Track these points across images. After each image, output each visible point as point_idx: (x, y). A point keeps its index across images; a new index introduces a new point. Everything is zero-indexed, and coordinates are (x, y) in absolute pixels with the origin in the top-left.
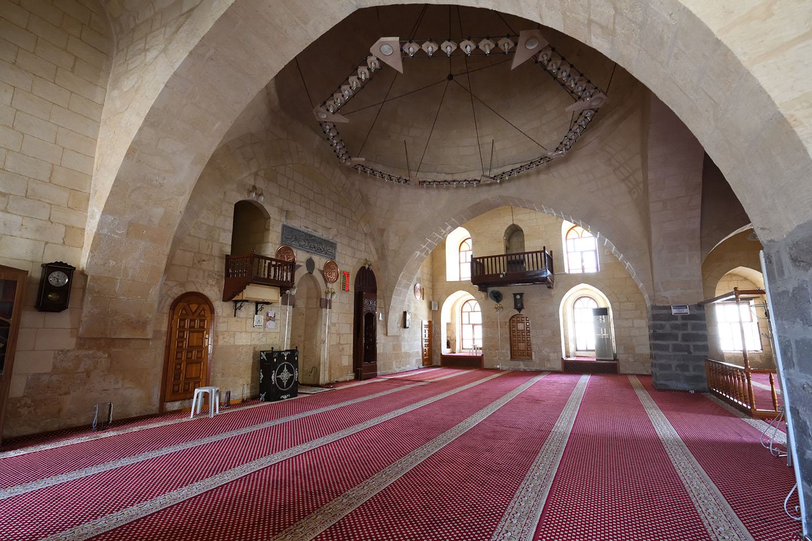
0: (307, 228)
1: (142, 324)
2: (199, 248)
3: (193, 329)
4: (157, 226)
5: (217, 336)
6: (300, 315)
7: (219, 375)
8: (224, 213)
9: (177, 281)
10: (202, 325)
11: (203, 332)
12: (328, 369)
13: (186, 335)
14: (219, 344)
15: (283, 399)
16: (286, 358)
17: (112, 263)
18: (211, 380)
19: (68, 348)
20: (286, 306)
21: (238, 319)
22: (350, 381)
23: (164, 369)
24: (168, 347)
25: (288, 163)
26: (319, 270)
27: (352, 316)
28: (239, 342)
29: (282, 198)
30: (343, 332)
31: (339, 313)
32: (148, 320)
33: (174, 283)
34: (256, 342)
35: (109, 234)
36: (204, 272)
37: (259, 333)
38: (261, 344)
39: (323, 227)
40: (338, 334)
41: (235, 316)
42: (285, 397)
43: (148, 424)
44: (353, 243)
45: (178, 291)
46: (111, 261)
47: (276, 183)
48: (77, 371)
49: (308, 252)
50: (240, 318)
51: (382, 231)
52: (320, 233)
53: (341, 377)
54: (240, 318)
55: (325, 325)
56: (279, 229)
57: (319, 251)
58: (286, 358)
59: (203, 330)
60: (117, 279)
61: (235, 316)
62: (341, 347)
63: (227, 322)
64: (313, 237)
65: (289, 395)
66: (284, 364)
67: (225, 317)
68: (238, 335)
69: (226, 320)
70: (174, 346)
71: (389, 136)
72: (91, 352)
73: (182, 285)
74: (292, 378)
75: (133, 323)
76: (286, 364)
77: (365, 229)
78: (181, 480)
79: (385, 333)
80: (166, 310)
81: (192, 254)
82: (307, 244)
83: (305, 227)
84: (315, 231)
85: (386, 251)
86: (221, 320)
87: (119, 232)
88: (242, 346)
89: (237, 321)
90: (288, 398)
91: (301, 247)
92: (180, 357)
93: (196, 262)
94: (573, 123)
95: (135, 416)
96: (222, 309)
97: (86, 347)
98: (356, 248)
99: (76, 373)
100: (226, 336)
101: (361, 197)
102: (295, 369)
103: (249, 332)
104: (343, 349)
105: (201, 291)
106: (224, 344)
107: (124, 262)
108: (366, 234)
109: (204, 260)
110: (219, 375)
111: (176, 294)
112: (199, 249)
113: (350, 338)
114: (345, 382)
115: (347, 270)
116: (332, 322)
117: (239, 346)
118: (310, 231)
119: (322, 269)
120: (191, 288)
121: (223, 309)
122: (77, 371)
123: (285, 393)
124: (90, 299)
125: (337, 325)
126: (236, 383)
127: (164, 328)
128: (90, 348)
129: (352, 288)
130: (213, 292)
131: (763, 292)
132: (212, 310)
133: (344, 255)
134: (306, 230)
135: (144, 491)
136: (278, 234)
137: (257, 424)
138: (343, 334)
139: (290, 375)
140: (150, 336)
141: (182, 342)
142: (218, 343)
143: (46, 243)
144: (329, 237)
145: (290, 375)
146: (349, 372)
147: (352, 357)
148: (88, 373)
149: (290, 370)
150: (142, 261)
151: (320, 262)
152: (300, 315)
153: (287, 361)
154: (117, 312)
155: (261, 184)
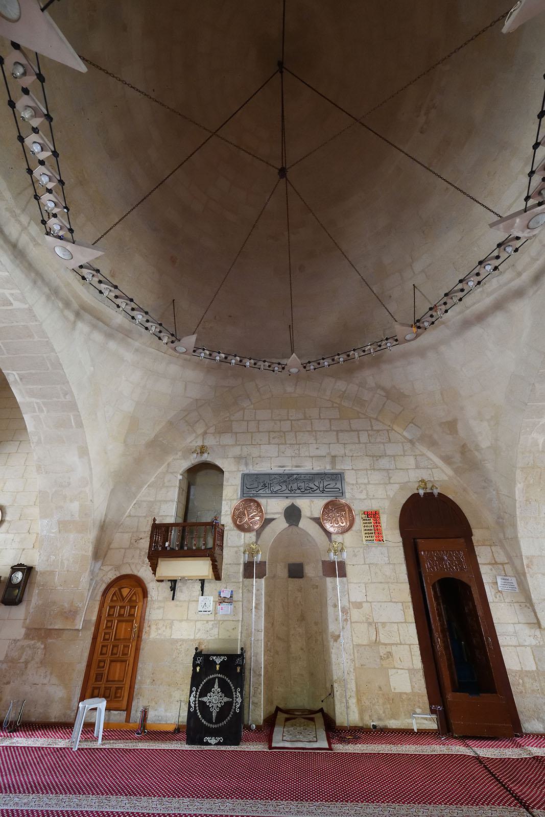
0: (283, 467)
1: (71, 614)
2: (138, 527)
3: (122, 618)
4: (78, 519)
5: (149, 626)
6: (313, 589)
7: (148, 681)
8: (167, 484)
9: (113, 565)
10: (132, 613)
11: (133, 622)
12: (353, 694)
14: (150, 637)
15: (208, 744)
16: (218, 667)
17: (53, 557)
18: (136, 687)
19: (18, 638)
20: (252, 579)
21: (178, 603)
22: (423, 734)
23: (87, 666)
24: (95, 639)
25: (245, 406)
26: (311, 519)
27: (407, 587)
28: (176, 635)
29: (239, 445)
30: (383, 619)
31: (366, 584)
32: (79, 609)
33: (110, 567)
34: (201, 636)
35: (48, 534)
36: (141, 550)
37: (207, 621)
38: (210, 638)
39: (312, 457)
40: (370, 624)
41: (173, 599)
42: (213, 741)
44: (384, 463)
45: (112, 576)
46: (51, 556)
47: (232, 432)
48: (19, 661)
49: (287, 497)
50: (180, 601)
51: (451, 426)
52: (309, 467)
53: (394, 716)
54: (180, 601)
55: (335, 606)
56: (238, 481)
57: (307, 492)
58: (218, 667)
59: (132, 618)
60: (56, 571)
61: (173, 599)
62: (383, 651)
63: (164, 607)
64: (295, 476)
65: (221, 739)
66: (215, 679)
67: (160, 601)
68: (176, 625)
69: (162, 605)
71: (390, 296)
72: (33, 642)
73: (117, 568)
75: (65, 612)
76: (218, 677)
77: (405, 434)
78: (486, 795)
81: (130, 534)
82: (284, 487)
83: (280, 467)
84: (297, 467)
85: (476, 453)
86: (156, 605)
87: (53, 531)
88: (183, 640)
89: (177, 606)
90: (218, 744)
91: (275, 494)
92: (105, 652)
93: (133, 541)
95: (54, 721)
97: (31, 637)
98: (392, 467)
99: (19, 663)
100: (160, 626)
101: (384, 394)
102: (236, 689)
103: (191, 621)
104: (389, 654)
105: (136, 573)
106: (157, 637)
107: (60, 555)
108: (411, 441)
109: (141, 538)
110: (148, 681)
111: (110, 579)
112: (138, 528)
113: (410, 633)
114: (405, 734)
115: (373, 506)
116: (353, 599)
117: (177, 641)
118: (289, 469)
119: (316, 515)
120: (126, 571)
121: (158, 591)
122: (19, 661)
124: (37, 592)
125: (365, 605)
126: (170, 696)
128: (33, 639)
130: (144, 572)
132: (145, 594)
133: (363, 486)
134: (280, 471)
135: (485, 790)
136: (235, 487)
137: (540, 747)
138: (384, 624)
139: (226, 699)
142: (149, 635)
143: (24, 549)
144: (325, 468)
145: (226, 699)
146: (418, 711)
147: (421, 673)
148: (26, 663)
149: (226, 690)
150: (74, 552)
151: (311, 506)
152: (313, 589)
153: (219, 672)
154: (55, 602)
155: (210, 441)
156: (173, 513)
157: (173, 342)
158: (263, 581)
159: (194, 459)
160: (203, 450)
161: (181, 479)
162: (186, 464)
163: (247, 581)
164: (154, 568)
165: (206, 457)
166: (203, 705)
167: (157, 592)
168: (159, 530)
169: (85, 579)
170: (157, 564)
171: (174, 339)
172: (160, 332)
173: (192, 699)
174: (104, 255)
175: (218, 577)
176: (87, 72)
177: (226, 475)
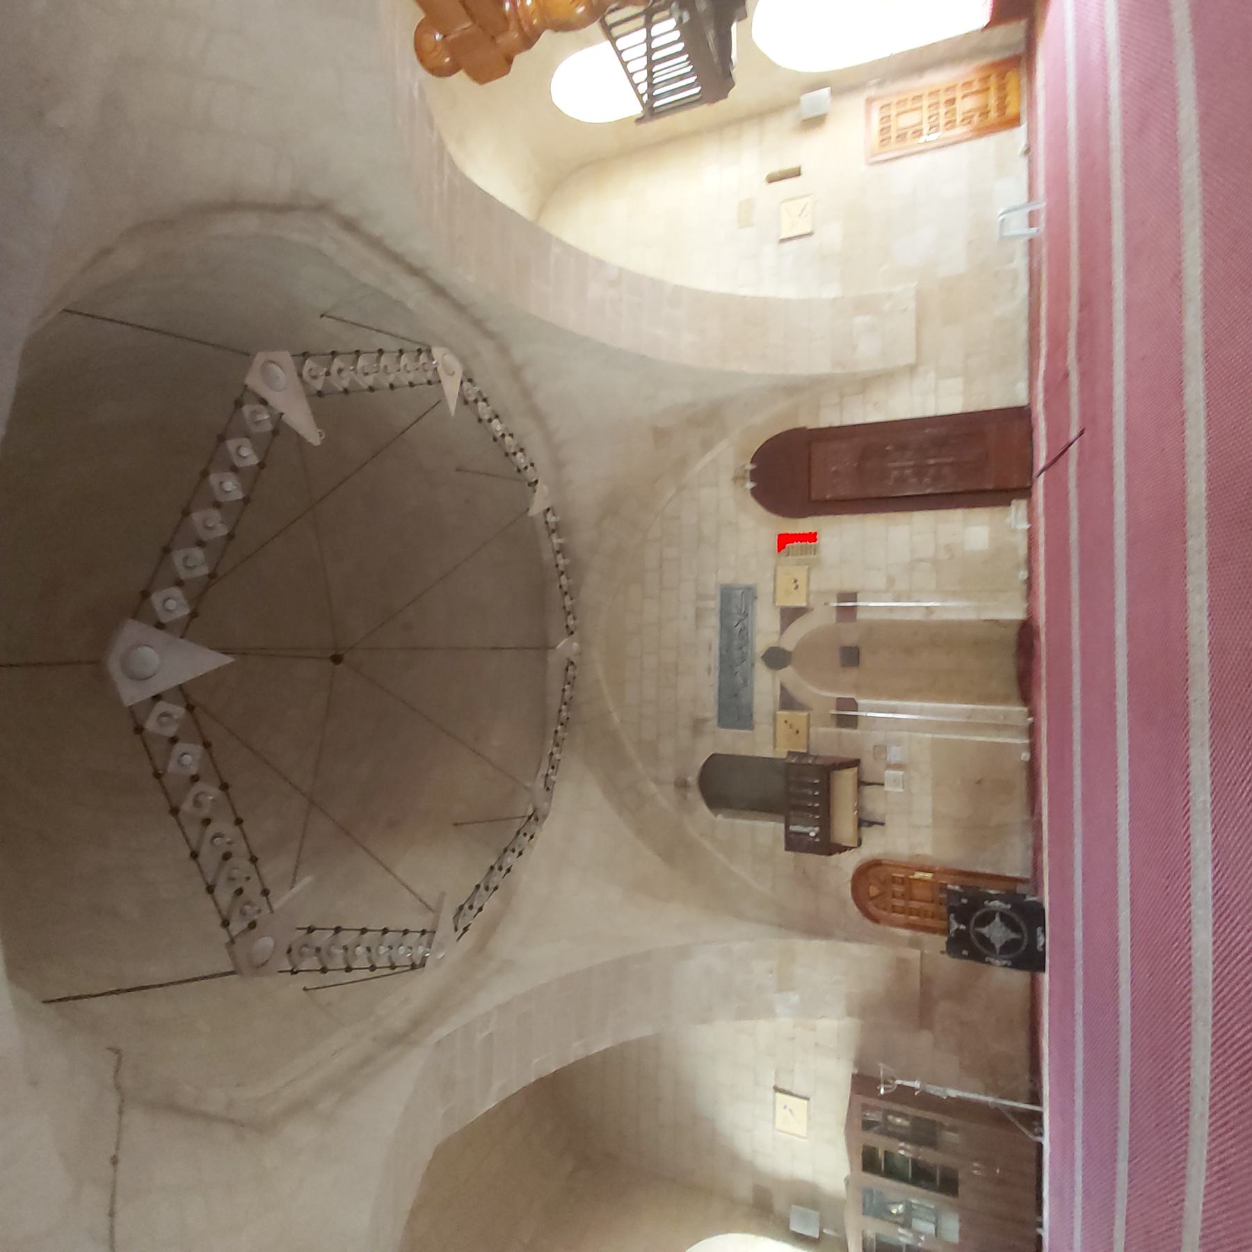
13: (915, 905)
22: (1031, 518)
43: (1039, 584)
51: (660, 435)
65: (1039, 930)
70: (929, 922)
74: (1004, 917)
79: (887, 108)
80: (879, 928)
83: (709, 673)
84: (710, 648)
90: (1044, 931)
94: (397, 970)
96: (875, 846)
123: (1033, 940)
127: (906, 933)
129: (803, 526)
131: (809, 715)
140: (917, 953)
141: (926, 911)
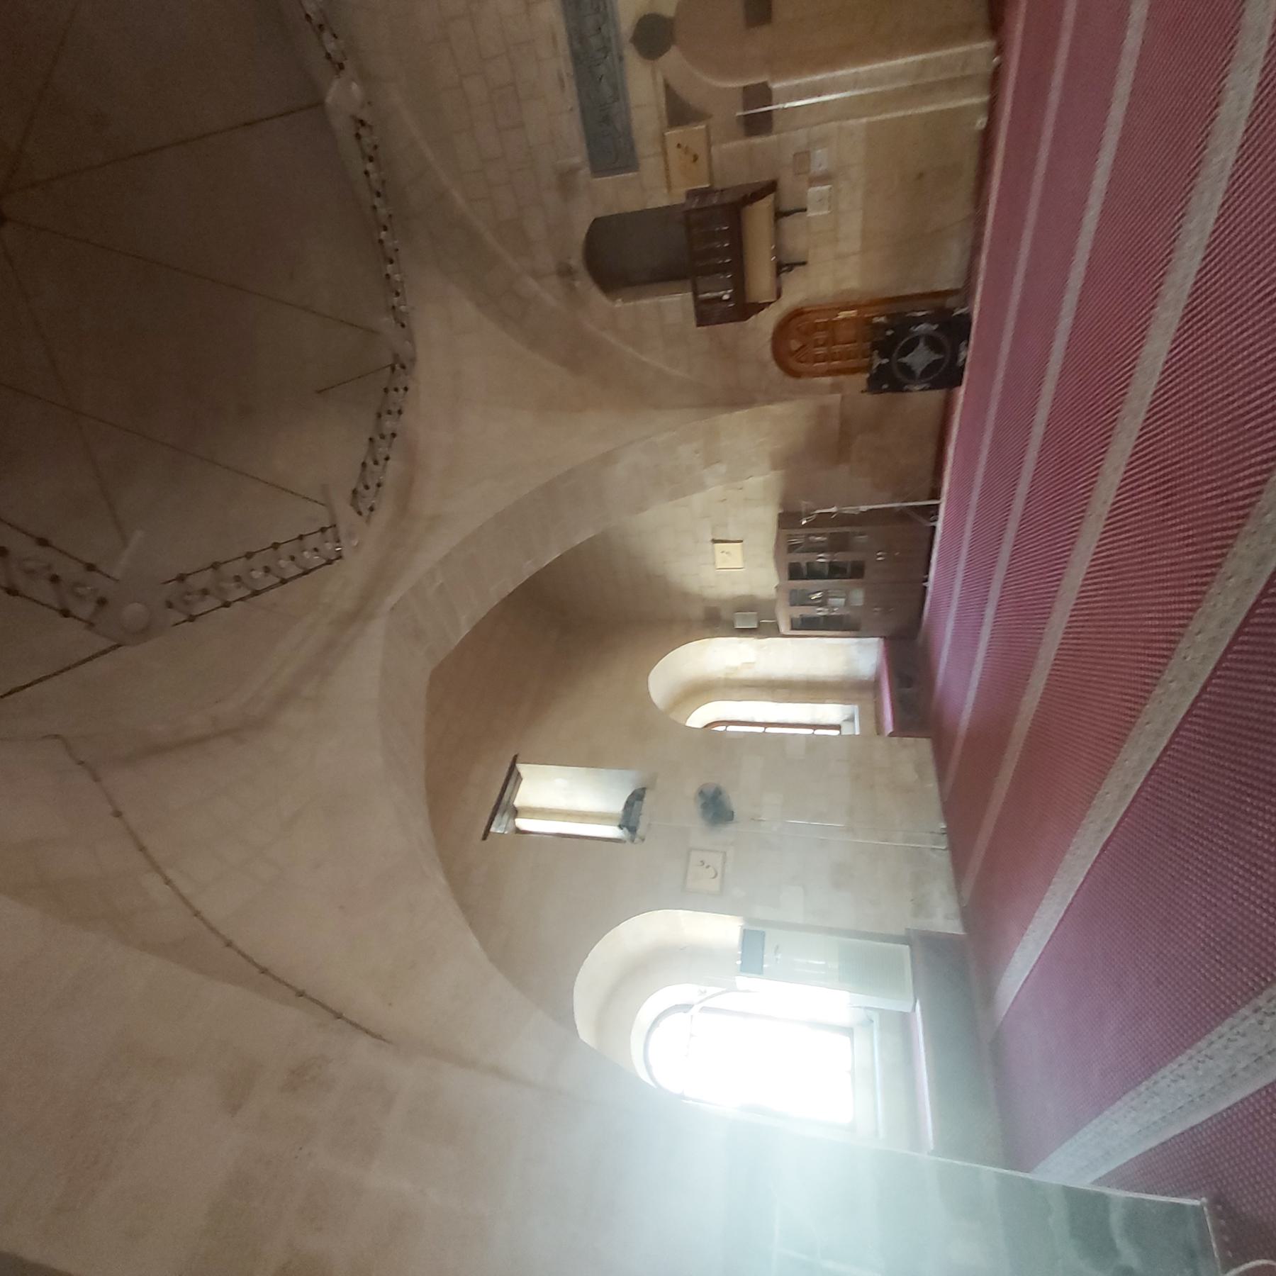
42: (963, 354)
58: (885, 361)
83: (563, 86)
105: (770, 337)
118: (566, 67)
130: (766, 321)
149: (910, 347)
156: (677, 298)
157: (403, 367)
158: (776, 86)
159: (585, 283)
160: (566, 272)
161: (623, 300)
162: (596, 297)
163: (778, 123)
164: (760, 307)
165: (576, 261)
166: (926, 372)
167: (798, 291)
168: (706, 315)
169: (777, 409)
170: (753, 303)
171: (397, 367)
172: (396, 390)
173: (917, 388)
174: (950, 938)
175: (771, 187)
176: (544, 759)
177: (601, 213)
